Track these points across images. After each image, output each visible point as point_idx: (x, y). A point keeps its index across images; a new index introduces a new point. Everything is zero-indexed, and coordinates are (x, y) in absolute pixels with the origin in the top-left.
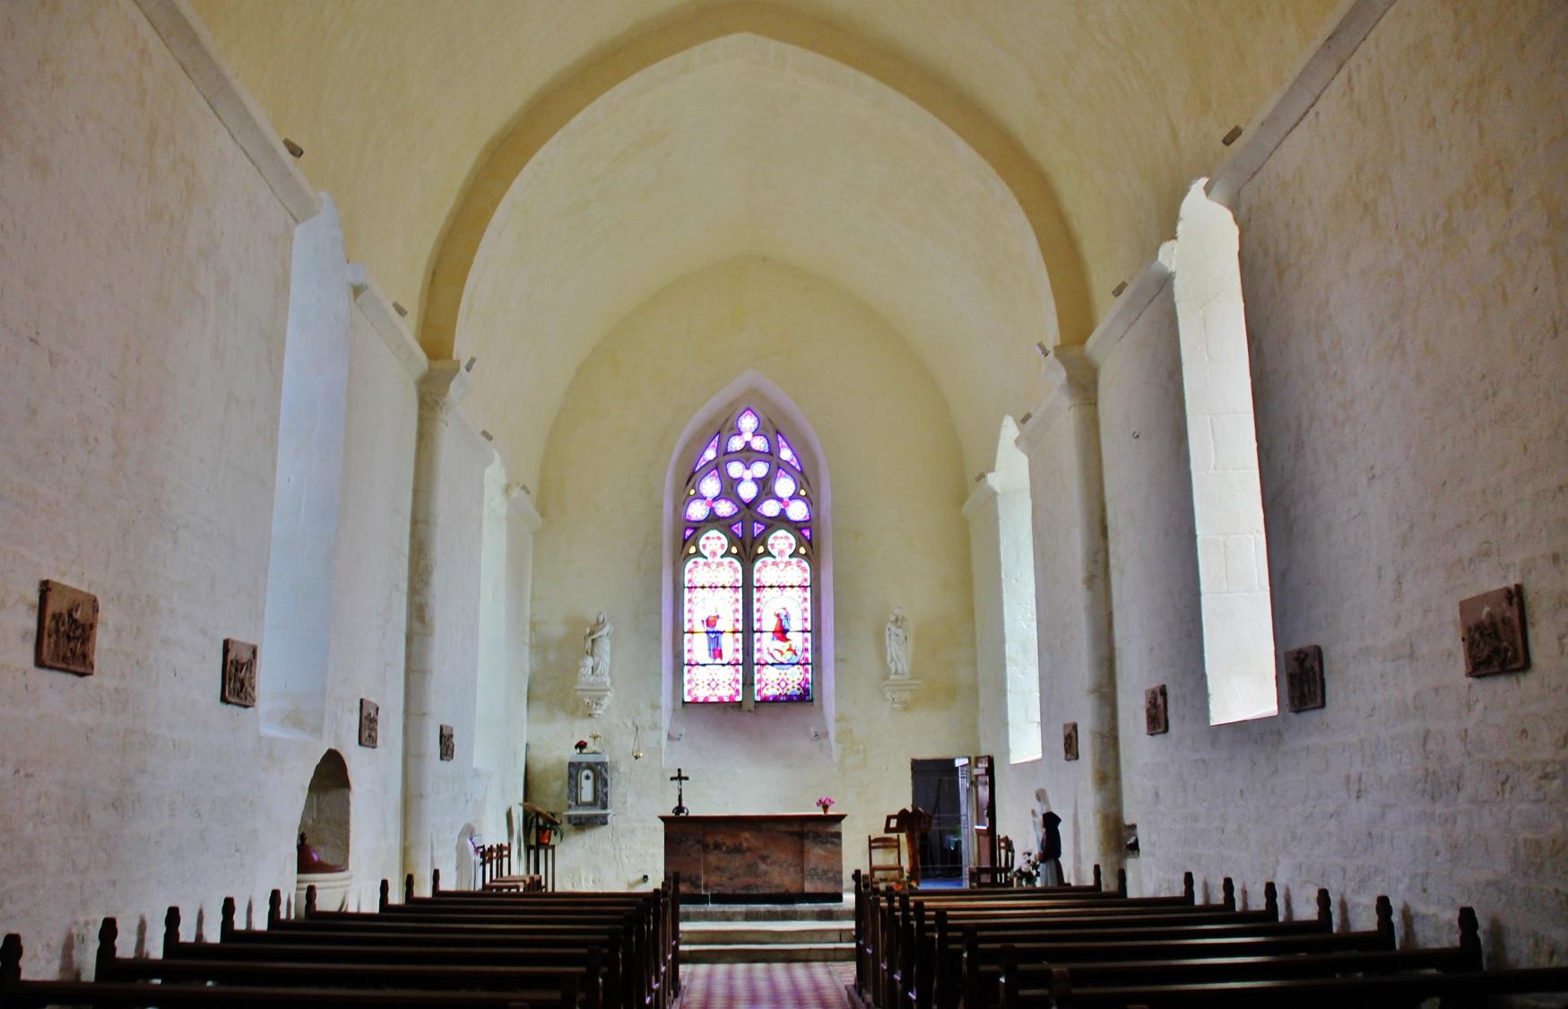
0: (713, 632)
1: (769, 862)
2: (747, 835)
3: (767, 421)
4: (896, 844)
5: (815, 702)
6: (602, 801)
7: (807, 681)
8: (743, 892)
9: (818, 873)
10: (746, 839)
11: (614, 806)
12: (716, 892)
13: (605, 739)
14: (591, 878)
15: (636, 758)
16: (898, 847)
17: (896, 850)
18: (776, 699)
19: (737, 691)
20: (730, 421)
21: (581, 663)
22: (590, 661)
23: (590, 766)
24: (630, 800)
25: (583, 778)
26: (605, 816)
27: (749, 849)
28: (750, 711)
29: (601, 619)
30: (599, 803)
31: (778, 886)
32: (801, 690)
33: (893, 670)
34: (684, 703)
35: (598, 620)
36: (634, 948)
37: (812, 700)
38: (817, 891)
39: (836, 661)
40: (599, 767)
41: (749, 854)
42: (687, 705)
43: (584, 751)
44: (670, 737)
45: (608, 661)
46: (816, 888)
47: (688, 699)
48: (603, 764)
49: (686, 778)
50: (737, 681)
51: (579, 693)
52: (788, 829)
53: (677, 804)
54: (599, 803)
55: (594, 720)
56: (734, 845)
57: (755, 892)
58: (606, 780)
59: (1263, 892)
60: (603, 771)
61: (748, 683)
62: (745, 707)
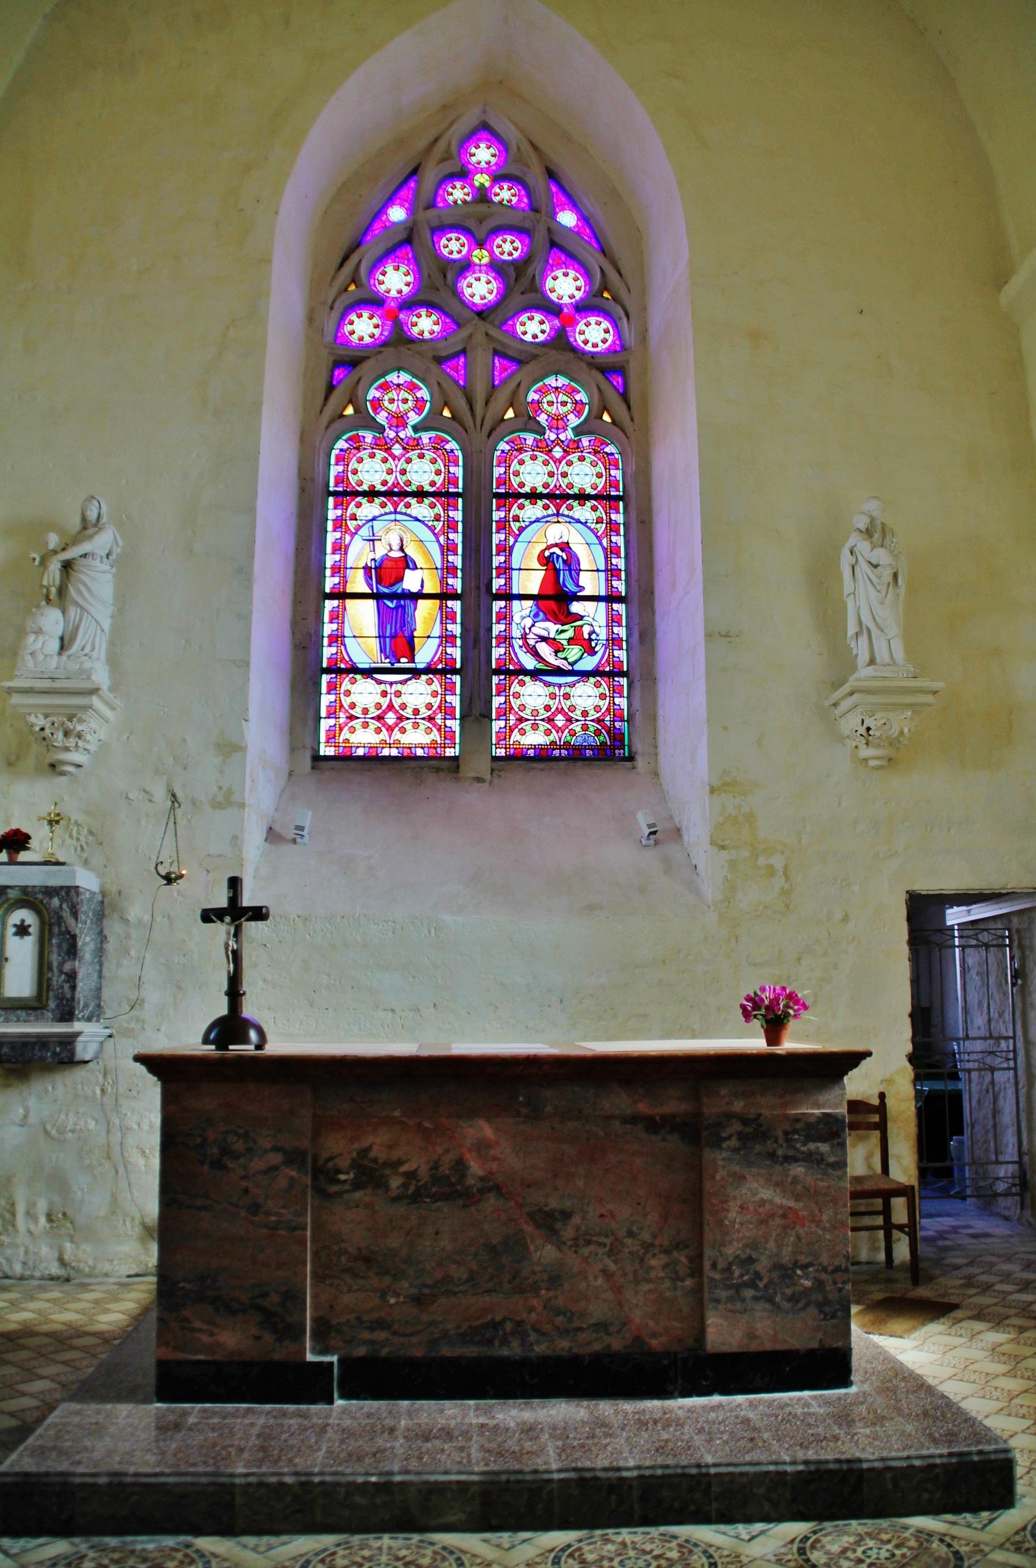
0: (392, 596)
1: (568, 1233)
2: (486, 1130)
3: (525, 146)
4: (876, 1118)
5: (640, 762)
6: (60, 999)
7: (618, 716)
8: (471, 1351)
9: (758, 1276)
10: (482, 1147)
11: (109, 1014)
12: (361, 1351)
13: (91, 832)
14: (42, 1206)
15: (169, 879)
16: (882, 1127)
17: (877, 1133)
18: (543, 755)
19: (449, 735)
20: (442, 145)
21: (29, 625)
22: (52, 620)
23: (28, 898)
24: (152, 996)
25: (11, 930)
26: (68, 1041)
27: (491, 1186)
28: (480, 780)
29: (92, 515)
30: (52, 1004)
31: (602, 1327)
32: (604, 737)
33: (863, 657)
34: (317, 758)
35: (84, 519)
36: (309, 1202)
37: (631, 758)
38: (754, 1347)
39: (709, 636)
40: (56, 902)
41: (491, 1201)
42: (322, 764)
43: (23, 856)
44: (272, 835)
45: (106, 624)
46: (751, 1335)
47: (326, 750)
48: (69, 893)
49: (259, 914)
50: (449, 712)
51: (16, 699)
52: (643, 1107)
53: (222, 1009)
54: (52, 1004)
55: (63, 780)
56: (435, 1166)
57: (513, 1350)
58: (74, 937)
59: (857, 1069)
60: (66, 913)
61: (476, 712)
62: (468, 771)
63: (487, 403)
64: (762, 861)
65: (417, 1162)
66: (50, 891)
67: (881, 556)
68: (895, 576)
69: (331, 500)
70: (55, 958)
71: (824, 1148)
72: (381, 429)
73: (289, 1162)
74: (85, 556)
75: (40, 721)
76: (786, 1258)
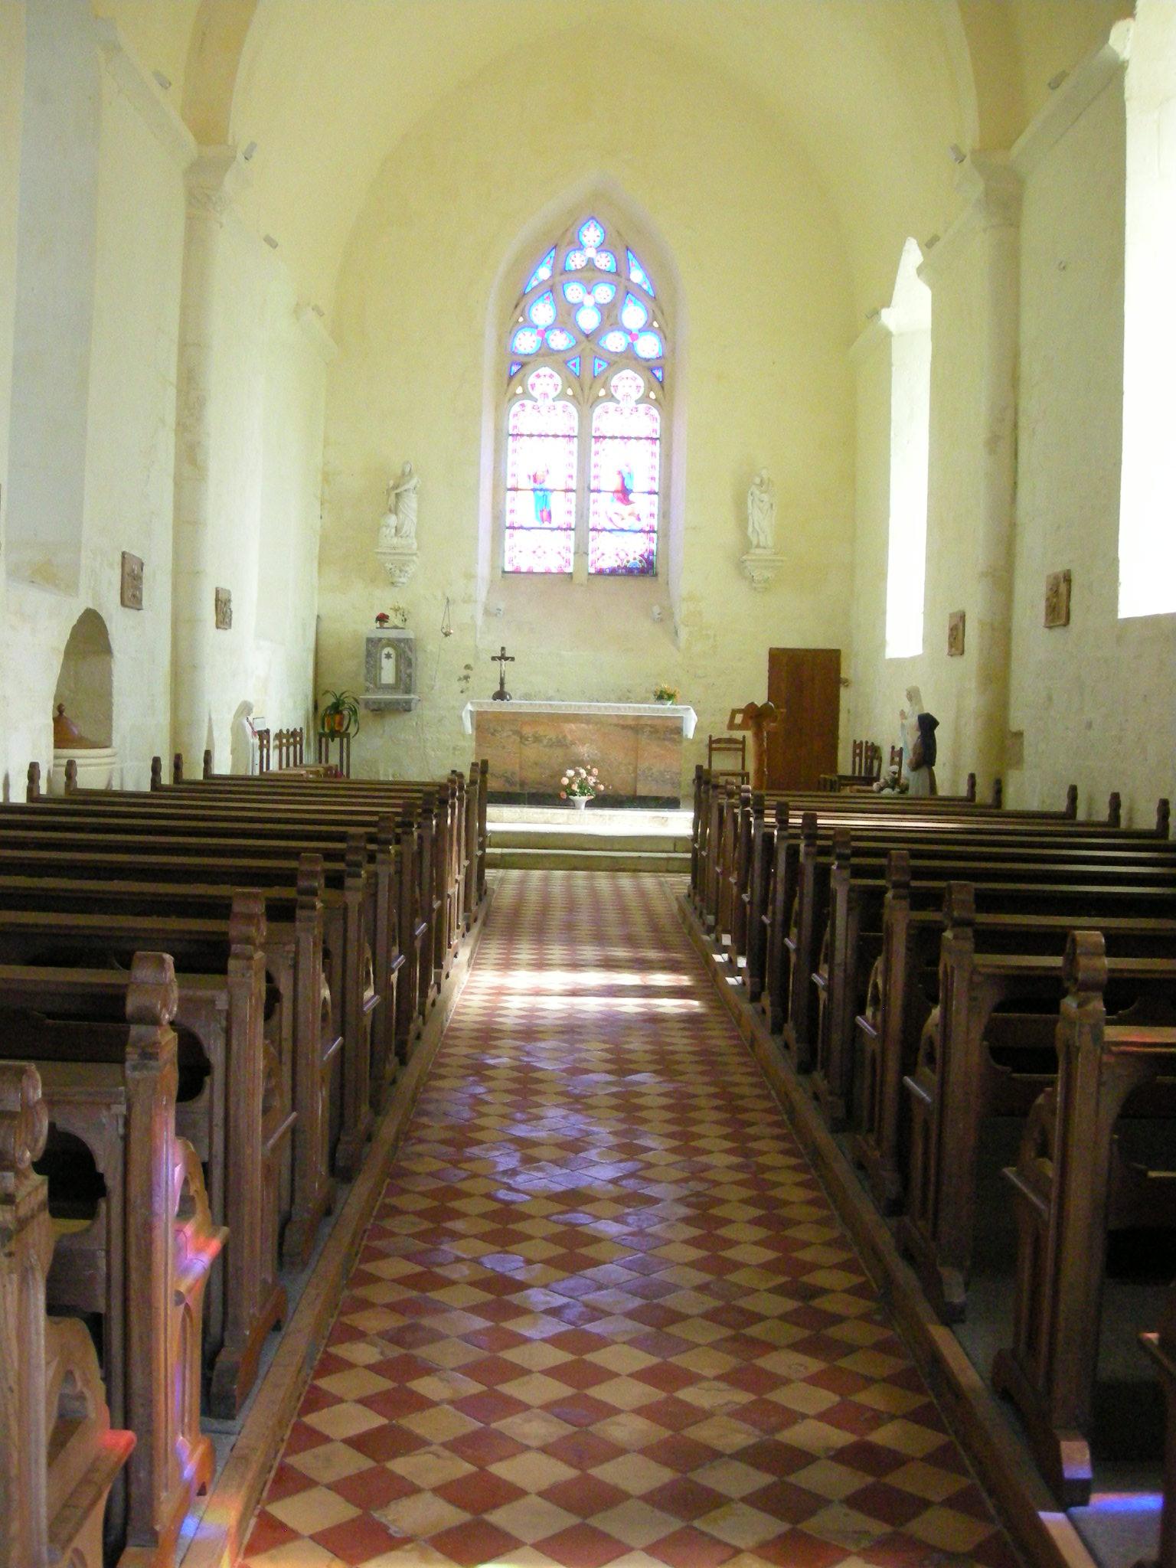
5: (660, 579)
16: (743, 750)
19: (568, 562)
22: (392, 520)
25: (383, 656)
26: (408, 702)
29: (407, 470)
30: (402, 687)
44: (487, 612)
45: (415, 519)
47: (508, 568)
53: (498, 688)
54: (402, 687)
55: (397, 589)
63: (590, 388)
64: (704, 632)
65: (552, 735)
66: (400, 640)
67: (765, 497)
68: (772, 505)
69: (510, 438)
70: (402, 668)
71: (676, 737)
72: (536, 400)
73: (514, 734)
74: (406, 490)
75: (389, 566)
76: (662, 769)
